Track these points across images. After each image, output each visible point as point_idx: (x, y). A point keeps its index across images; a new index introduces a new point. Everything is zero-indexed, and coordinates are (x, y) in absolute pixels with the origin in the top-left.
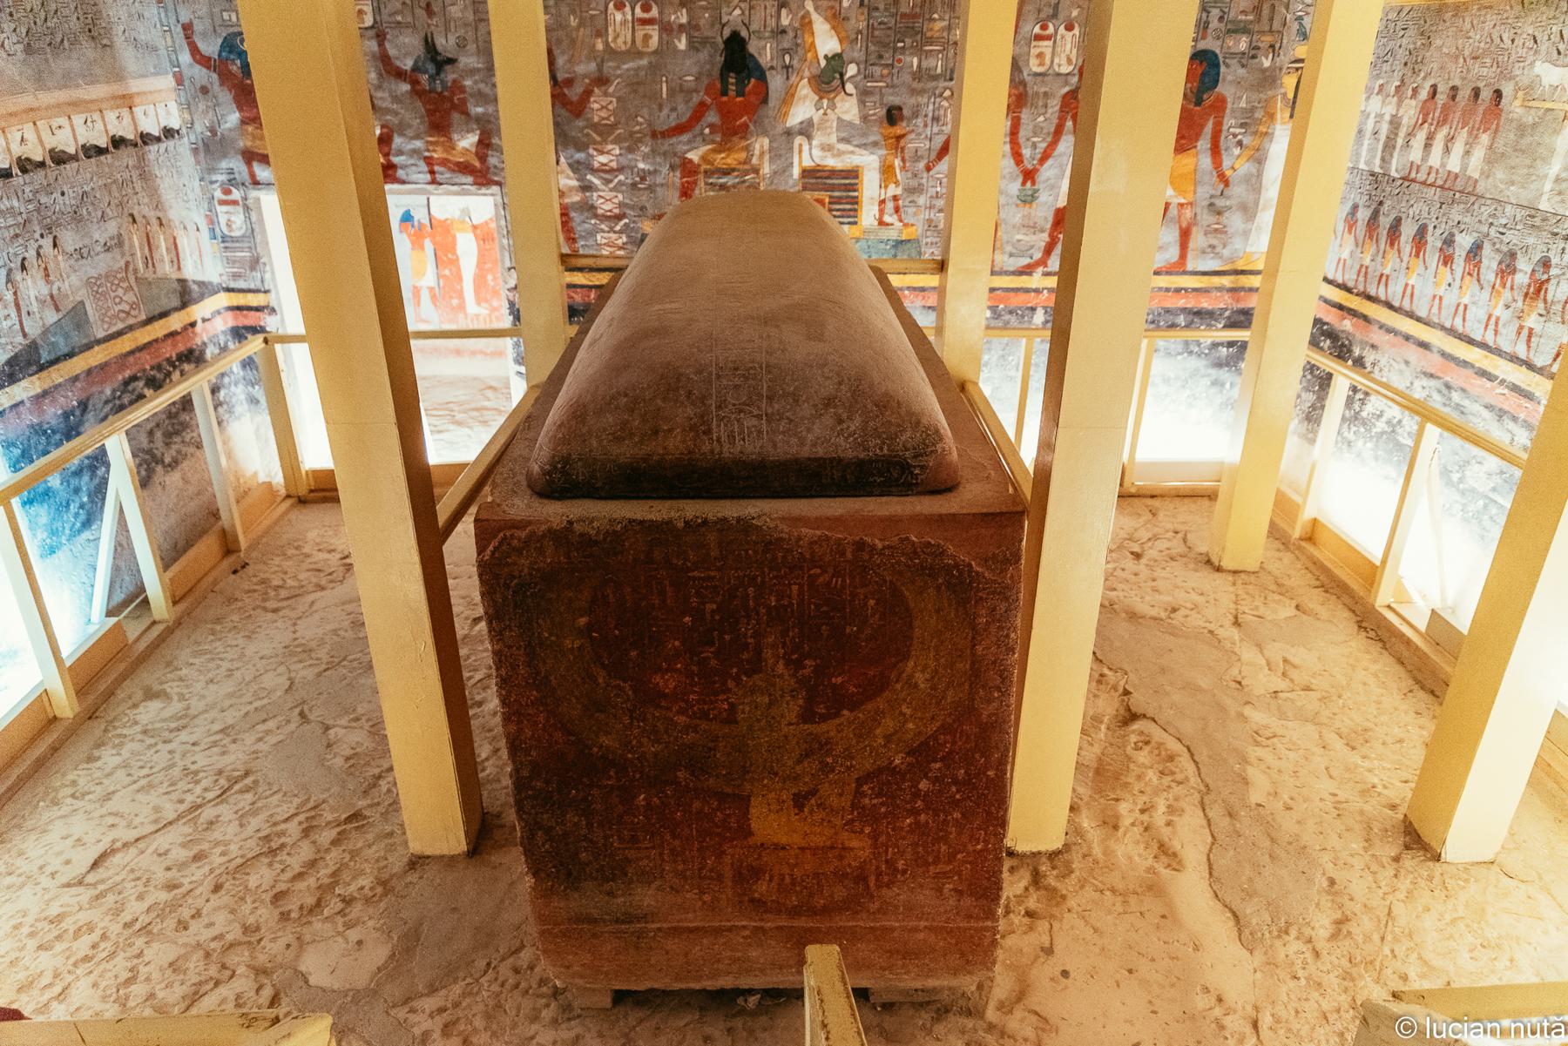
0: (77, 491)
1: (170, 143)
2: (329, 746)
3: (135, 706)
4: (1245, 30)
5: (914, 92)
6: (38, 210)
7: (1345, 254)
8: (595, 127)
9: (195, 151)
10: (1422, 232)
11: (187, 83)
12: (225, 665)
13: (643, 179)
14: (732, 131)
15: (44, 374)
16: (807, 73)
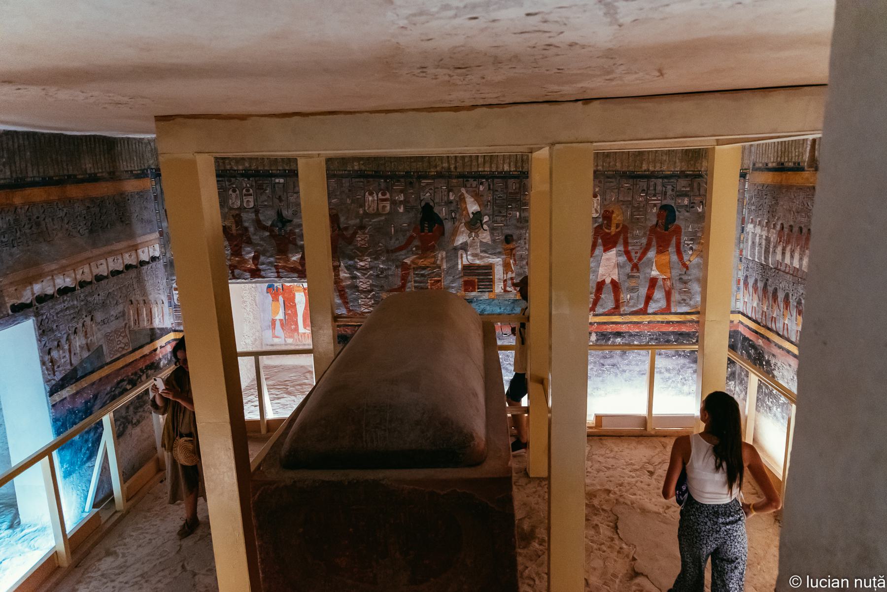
0: (87, 441)
1: (154, 264)
2: (194, 585)
3: (100, 560)
4: (686, 195)
5: (518, 228)
6: (86, 304)
7: (755, 305)
8: (358, 249)
9: (165, 266)
10: (787, 297)
12: (148, 536)
13: (382, 272)
14: (427, 249)
15: (77, 383)
16: (463, 221)
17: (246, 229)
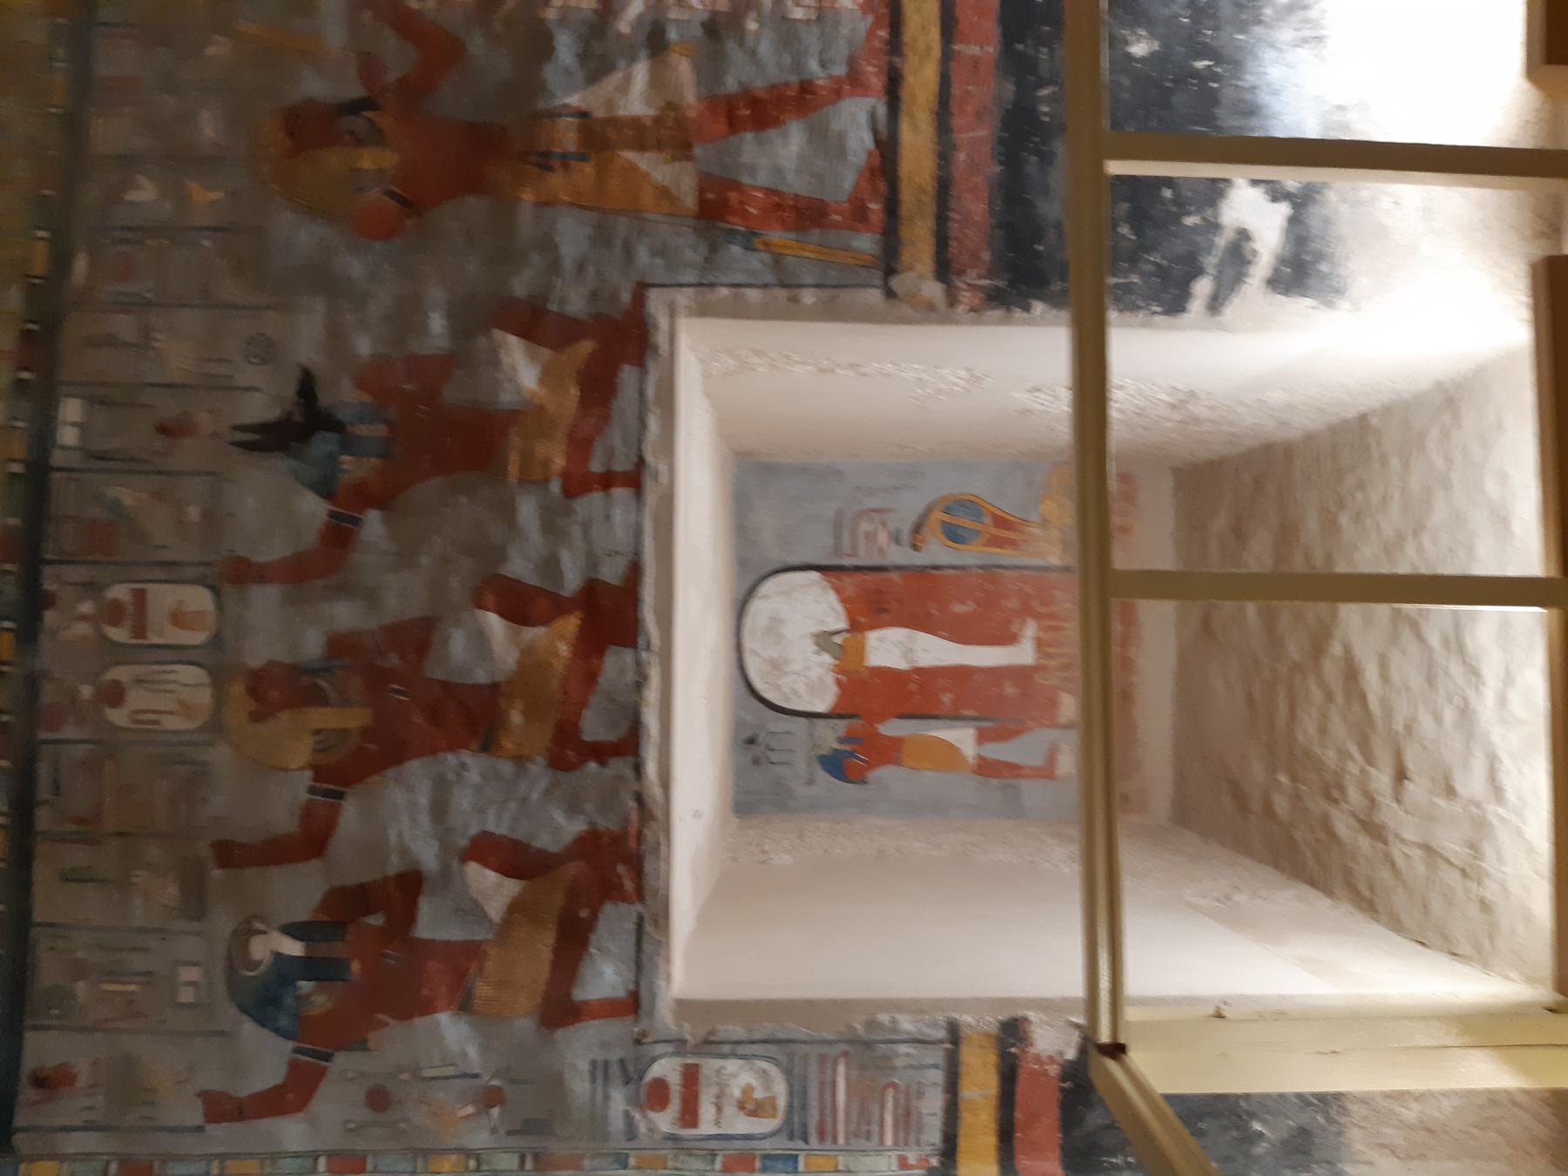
11: (360, 1145)
17: (340, 646)
